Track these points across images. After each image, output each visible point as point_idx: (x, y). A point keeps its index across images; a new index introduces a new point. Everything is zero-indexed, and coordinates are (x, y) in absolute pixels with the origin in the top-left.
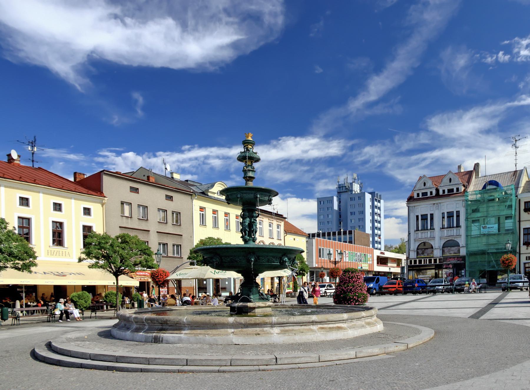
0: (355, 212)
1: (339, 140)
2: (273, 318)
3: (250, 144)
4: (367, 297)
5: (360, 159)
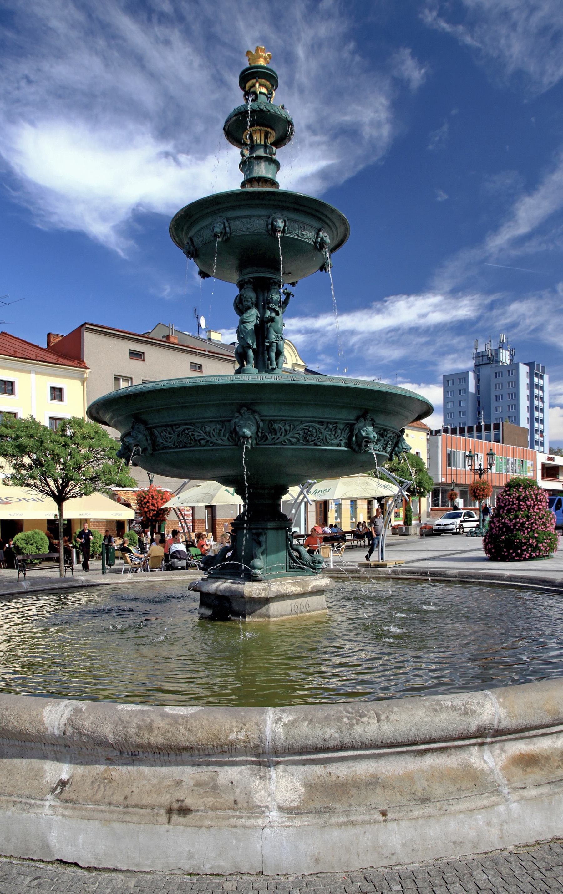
0: (502, 396)
2: (271, 714)
3: (263, 81)
4: (556, 539)
5: (504, 321)
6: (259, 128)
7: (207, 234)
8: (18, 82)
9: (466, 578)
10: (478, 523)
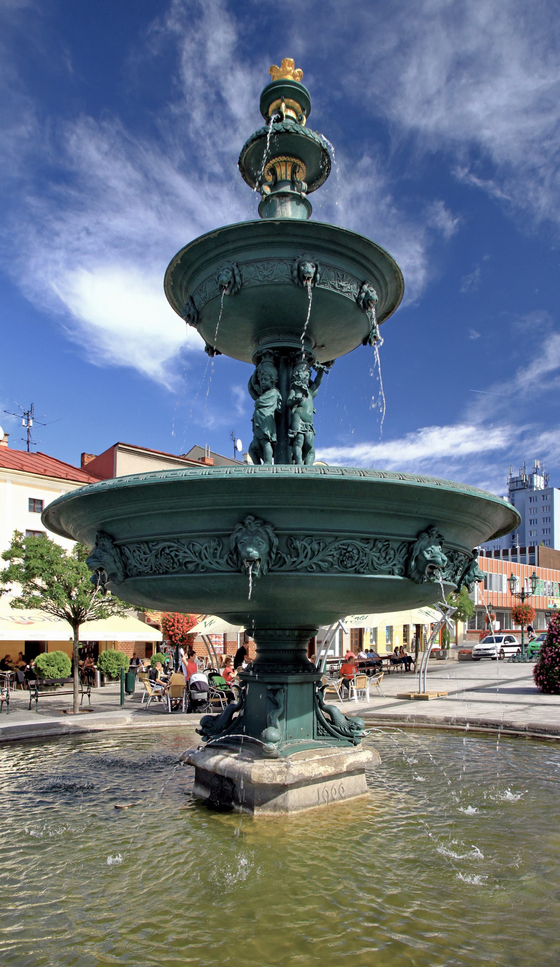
0: (536, 520)
1: (503, 427)
6: (284, 158)
7: (211, 288)
8: (79, 233)
9: (539, 733)
10: (519, 648)
